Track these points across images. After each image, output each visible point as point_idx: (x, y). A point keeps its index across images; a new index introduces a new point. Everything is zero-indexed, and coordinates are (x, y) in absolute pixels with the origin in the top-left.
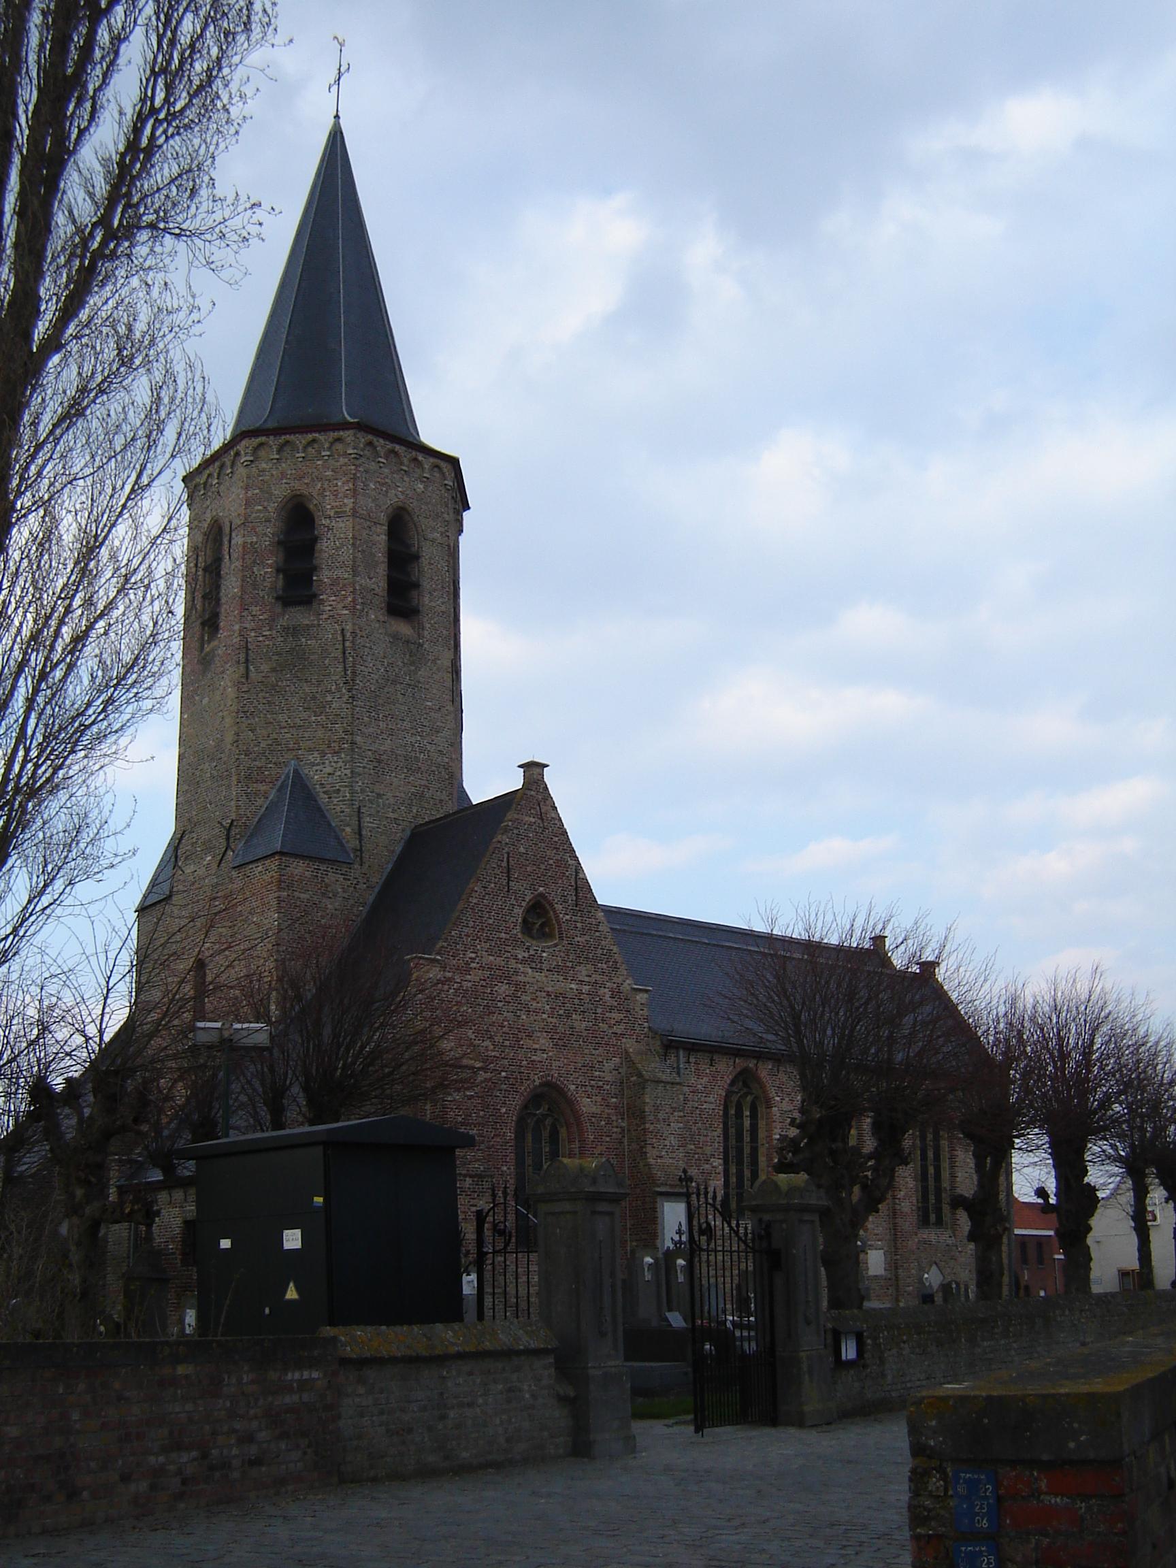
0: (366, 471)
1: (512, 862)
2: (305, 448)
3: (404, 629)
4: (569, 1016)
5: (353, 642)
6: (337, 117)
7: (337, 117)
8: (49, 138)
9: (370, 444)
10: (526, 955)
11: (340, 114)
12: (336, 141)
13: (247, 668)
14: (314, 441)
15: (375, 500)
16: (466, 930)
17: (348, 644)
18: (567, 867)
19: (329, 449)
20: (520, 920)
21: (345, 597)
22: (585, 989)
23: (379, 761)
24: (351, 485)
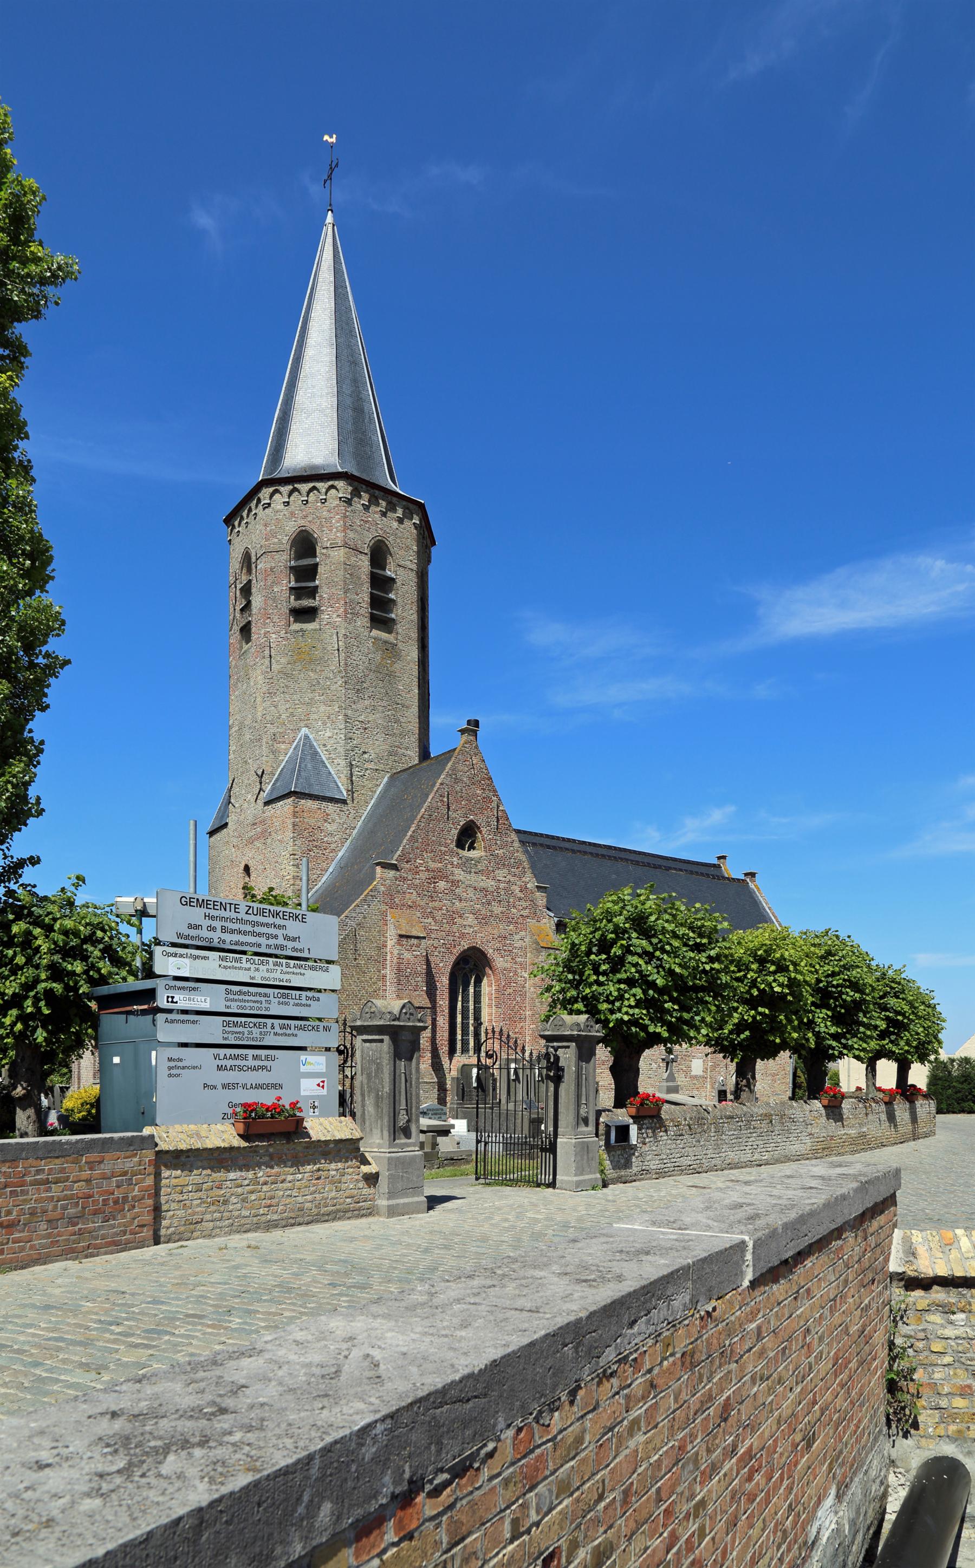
4: (489, 904)
8: (330, 218)
14: (314, 488)
17: (340, 643)
22: (502, 885)
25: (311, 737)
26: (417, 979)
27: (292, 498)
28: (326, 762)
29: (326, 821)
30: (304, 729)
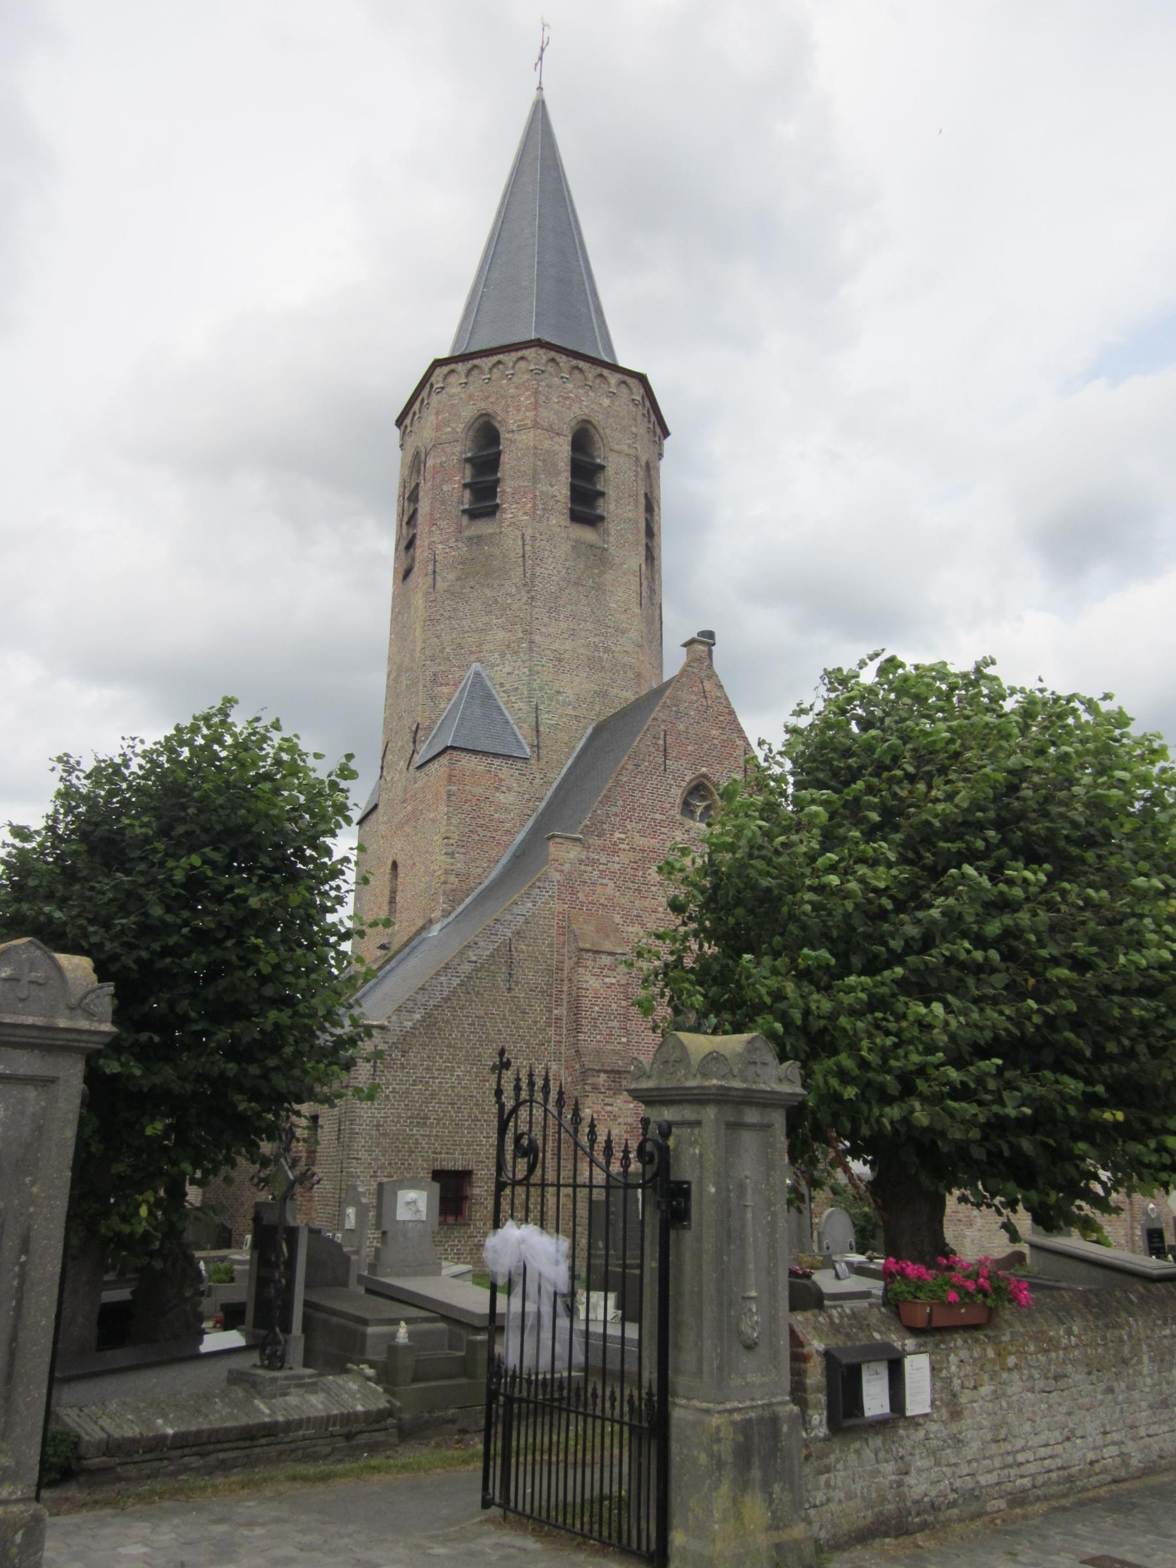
0: (549, 386)
1: (669, 740)
2: (491, 370)
3: (587, 534)
5: (532, 546)
6: (540, 88)
7: (540, 88)
9: (553, 360)
10: (686, 837)
11: (543, 86)
12: (540, 111)
13: (434, 579)
14: (499, 362)
15: (557, 413)
16: (615, 809)
17: (528, 548)
18: (735, 748)
19: (513, 367)
20: (678, 801)
21: (526, 503)
23: (560, 660)
24: (533, 399)
25: (484, 674)
26: (611, 1024)
27: (471, 379)
28: (503, 707)
29: (497, 789)
30: (474, 665)
